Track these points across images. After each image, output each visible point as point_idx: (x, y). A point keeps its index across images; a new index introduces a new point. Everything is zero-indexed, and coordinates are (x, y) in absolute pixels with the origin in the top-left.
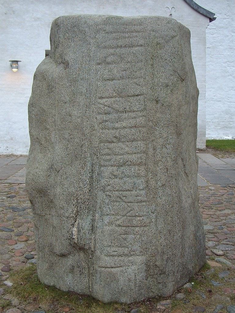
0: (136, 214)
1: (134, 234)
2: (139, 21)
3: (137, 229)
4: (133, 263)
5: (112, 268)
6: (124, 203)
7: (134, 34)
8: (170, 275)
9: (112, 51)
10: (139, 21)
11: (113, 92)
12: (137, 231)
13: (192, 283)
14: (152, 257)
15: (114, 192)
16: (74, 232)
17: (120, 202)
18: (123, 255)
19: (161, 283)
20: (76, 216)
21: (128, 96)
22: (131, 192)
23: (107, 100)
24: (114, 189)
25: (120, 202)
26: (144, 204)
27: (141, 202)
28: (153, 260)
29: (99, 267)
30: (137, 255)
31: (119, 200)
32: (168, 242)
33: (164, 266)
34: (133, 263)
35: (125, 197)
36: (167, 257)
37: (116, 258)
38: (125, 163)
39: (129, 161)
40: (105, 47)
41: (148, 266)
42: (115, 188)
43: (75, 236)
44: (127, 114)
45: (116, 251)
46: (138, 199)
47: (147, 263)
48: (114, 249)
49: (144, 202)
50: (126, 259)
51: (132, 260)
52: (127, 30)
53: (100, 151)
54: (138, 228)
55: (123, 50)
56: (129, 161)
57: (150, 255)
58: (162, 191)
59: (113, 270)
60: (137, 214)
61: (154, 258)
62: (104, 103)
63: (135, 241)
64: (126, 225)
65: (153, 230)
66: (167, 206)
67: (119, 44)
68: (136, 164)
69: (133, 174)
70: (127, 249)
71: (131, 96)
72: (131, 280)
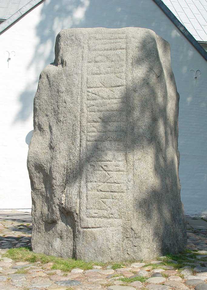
0: (115, 181)
1: (113, 199)
2: (123, 31)
3: (115, 194)
4: (111, 225)
5: (93, 228)
6: (104, 172)
7: (119, 40)
8: (145, 241)
9: (100, 53)
10: (123, 31)
11: (99, 83)
12: (115, 196)
13: (153, 25)
14: (128, 220)
15: (97, 162)
16: (63, 198)
17: (101, 171)
18: (103, 217)
19: (136, 246)
20: (65, 184)
21: (112, 87)
22: (111, 162)
23: (94, 89)
24: (97, 160)
25: (101, 171)
26: (122, 173)
27: (119, 171)
28: (129, 223)
29: (82, 228)
30: (115, 218)
31: (101, 169)
32: (143, 209)
33: (139, 231)
34: (111, 225)
35: (106, 167)
36: (142, 223)
37: (96, 219)
38: (107, 139)
39: (110, 137)
40: (95, 50)
41: (125, 229)
42: (98, 159)
43: (63, 201)
44: (110, 100)
45: (97, 213)
46: (117, 169)
47: (123, 225)
48: (96, 211)
49: (121, 171)
50: (105, 220)
51: (110, 222)
52: (113, 37)
53: (87, 129)
54: (116, 193)
55: (109, 52)
56: (110, 137)
57: (127, 218)
58: (138, 164)
59: (93, 229)
60: (115, 181)
61: (129, 222)
62: (92, 91)
63: (113, 205)
64: (106, 190)
65: (129, 197)
66: (142, 177)
67: (106, 48)
68: (116, 140)
69: (113, 148)
70: (106, 212)
71: (114, 87)
72: (109, 239)
